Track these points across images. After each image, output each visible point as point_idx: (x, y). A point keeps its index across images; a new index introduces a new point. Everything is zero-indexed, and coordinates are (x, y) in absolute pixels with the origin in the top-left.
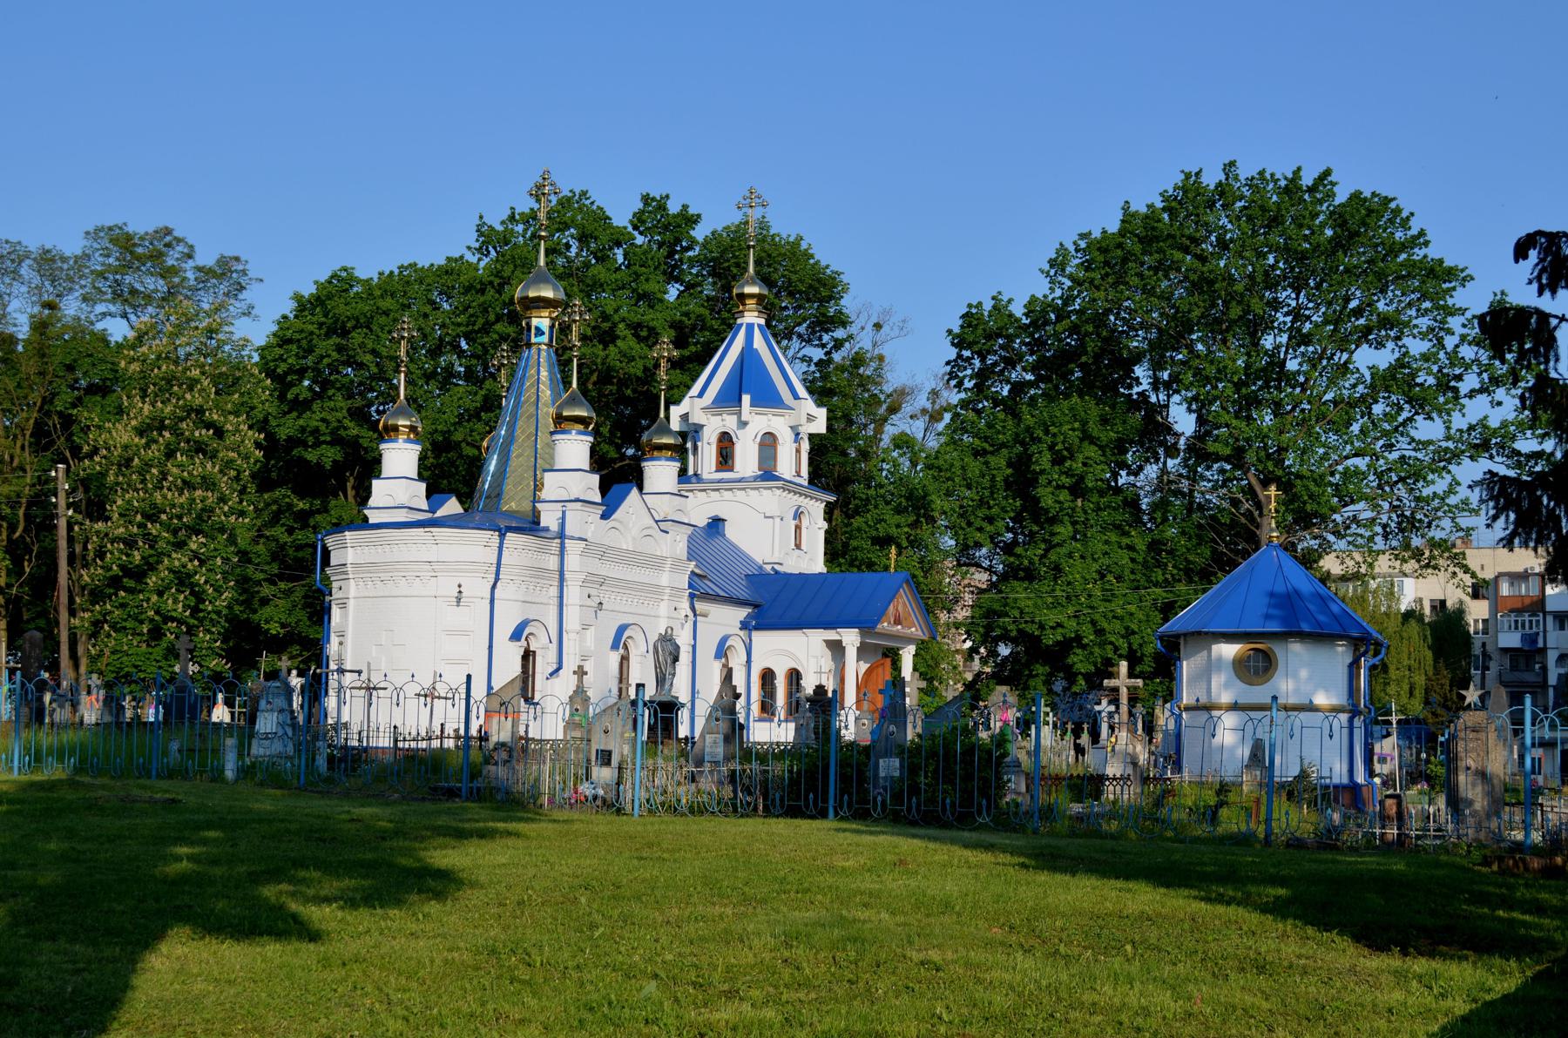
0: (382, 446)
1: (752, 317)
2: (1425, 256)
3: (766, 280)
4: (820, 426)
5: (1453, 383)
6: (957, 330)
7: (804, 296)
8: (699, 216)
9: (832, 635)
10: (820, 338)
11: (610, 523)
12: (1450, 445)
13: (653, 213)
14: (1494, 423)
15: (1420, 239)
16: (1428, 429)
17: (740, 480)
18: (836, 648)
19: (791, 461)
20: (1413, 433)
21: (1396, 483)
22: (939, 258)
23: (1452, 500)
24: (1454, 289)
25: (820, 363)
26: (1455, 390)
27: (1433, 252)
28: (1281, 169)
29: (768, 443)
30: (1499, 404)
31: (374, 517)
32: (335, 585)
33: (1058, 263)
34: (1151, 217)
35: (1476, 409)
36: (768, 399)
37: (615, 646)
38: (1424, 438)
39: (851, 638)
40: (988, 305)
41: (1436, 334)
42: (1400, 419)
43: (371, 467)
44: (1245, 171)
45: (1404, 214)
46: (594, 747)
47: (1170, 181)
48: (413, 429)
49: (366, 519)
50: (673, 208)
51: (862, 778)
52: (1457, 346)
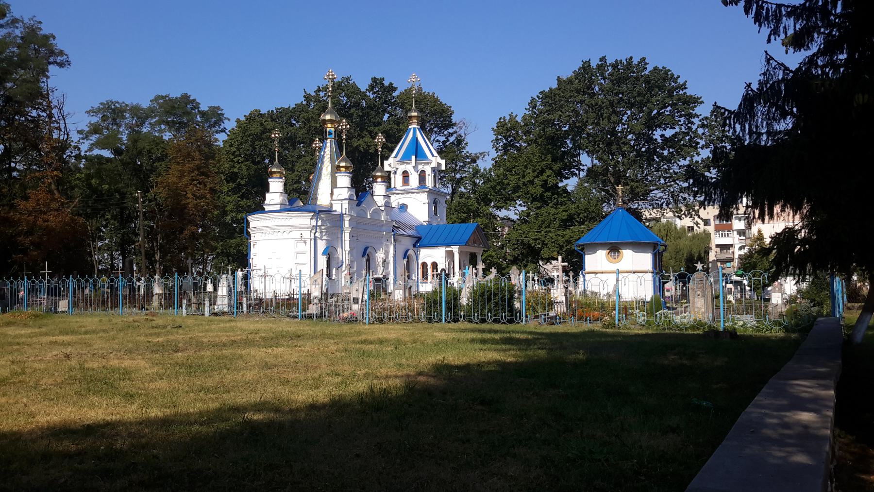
1: (414, 126)
3: (421, 111)
7: (437, 118)
9: (449, 249)
13: (376, 83)
15: (683, 87)
18: (450, 255)
22: (489, 101)
25: (444, 142)
27: (689, 92)
28: (623, 58)
29: (422, 176)
31: (267, 208)
33: (158, 98)
34: (570, 81)
37: (363, 256)
39: (455, 249)
40: (508, 118)
44: (610, 60)
47: (577, 65)
49: (264, 209)
50: (386, 83)
51: (455, 306)
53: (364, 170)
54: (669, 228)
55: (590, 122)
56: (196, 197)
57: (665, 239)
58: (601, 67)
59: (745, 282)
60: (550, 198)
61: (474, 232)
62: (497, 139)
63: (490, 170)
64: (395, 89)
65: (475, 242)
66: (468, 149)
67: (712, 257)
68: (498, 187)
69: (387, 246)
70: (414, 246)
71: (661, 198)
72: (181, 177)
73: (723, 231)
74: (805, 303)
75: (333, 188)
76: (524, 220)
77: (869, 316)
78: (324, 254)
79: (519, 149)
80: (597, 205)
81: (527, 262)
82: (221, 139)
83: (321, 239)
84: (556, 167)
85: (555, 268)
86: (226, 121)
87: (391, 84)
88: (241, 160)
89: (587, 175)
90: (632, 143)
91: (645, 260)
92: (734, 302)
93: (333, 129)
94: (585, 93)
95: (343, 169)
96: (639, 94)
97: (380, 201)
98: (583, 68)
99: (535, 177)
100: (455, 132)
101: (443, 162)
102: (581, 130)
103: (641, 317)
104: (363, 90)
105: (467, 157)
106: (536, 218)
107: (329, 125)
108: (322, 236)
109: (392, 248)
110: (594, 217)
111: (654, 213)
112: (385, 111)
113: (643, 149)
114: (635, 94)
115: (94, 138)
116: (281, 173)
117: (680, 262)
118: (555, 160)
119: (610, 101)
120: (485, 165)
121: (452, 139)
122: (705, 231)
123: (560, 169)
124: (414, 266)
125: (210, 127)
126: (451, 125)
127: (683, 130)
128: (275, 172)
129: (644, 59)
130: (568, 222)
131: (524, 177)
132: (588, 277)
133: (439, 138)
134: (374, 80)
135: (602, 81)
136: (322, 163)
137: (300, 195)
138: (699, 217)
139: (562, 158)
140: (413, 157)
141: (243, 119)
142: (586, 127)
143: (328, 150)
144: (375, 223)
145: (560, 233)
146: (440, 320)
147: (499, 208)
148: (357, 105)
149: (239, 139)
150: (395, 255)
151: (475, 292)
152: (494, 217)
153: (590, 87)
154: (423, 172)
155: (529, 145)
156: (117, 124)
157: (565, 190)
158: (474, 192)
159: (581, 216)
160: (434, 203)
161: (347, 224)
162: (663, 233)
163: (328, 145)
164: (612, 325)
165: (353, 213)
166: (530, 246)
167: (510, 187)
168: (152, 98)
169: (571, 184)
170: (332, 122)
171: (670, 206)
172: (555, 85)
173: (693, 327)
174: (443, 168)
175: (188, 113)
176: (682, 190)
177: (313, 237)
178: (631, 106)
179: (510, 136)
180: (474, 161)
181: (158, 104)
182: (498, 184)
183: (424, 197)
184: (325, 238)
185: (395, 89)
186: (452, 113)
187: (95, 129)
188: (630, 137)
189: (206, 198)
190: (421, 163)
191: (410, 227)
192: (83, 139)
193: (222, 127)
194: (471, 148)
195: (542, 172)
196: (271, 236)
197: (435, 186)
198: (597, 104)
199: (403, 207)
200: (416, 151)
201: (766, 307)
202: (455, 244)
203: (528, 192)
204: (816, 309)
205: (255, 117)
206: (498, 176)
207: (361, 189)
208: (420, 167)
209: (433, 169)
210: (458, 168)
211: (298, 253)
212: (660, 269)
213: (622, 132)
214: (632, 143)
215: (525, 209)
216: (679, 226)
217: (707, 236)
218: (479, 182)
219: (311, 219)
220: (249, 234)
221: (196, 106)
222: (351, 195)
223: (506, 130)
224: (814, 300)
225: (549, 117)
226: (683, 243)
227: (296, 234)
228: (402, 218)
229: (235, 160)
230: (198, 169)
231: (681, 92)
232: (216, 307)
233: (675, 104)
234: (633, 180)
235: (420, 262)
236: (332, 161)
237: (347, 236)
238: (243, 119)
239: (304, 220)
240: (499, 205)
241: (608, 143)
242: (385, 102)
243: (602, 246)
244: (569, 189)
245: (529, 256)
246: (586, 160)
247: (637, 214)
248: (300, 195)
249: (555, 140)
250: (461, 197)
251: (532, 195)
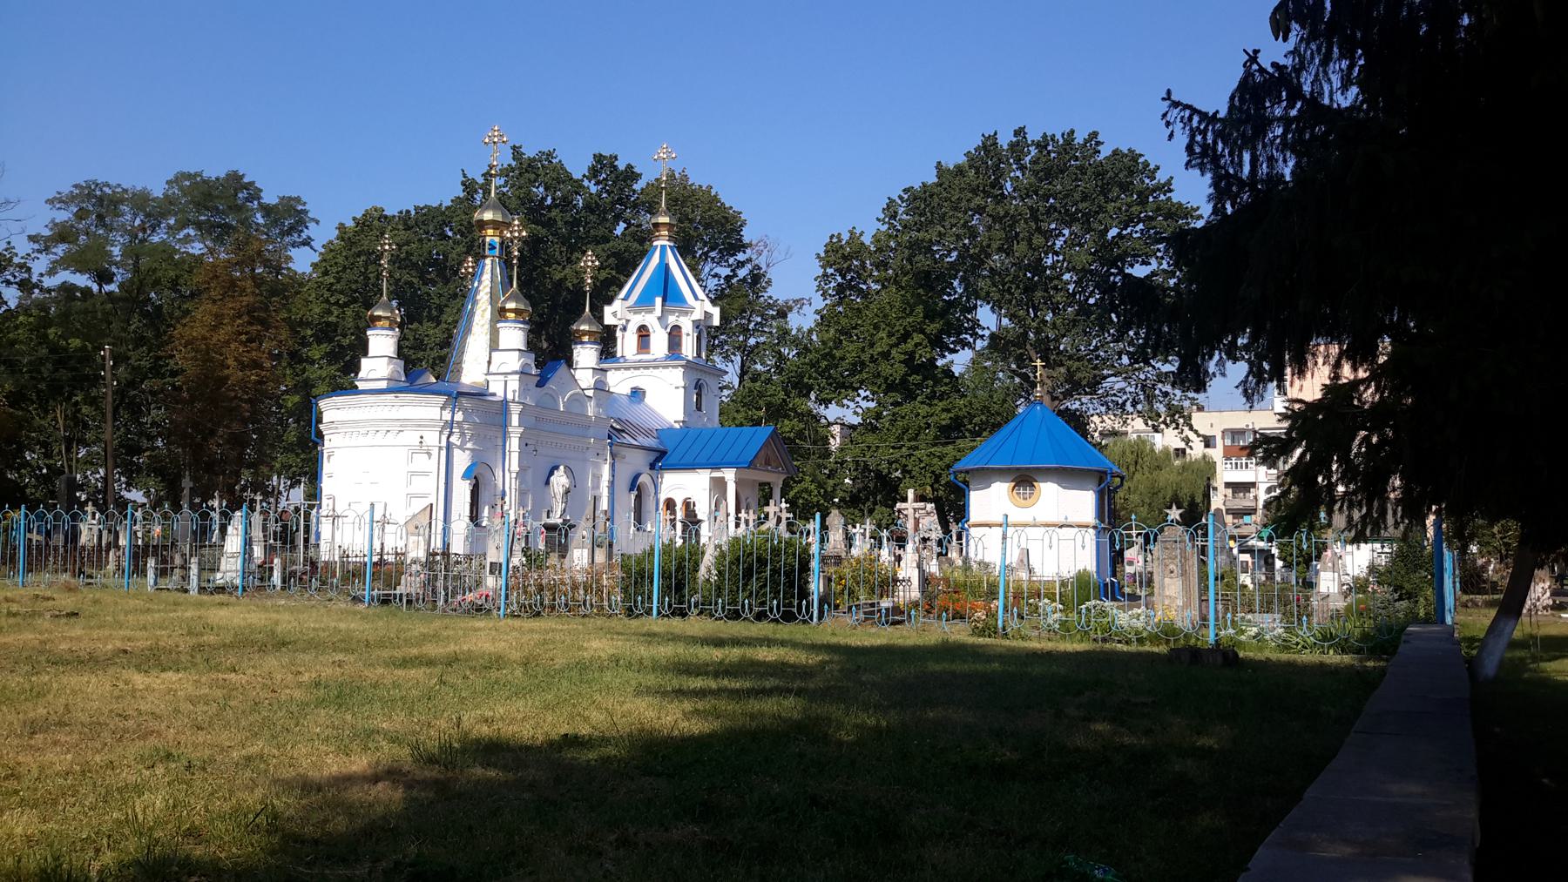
1: (662, 241)
7: (709, 231)
9: (717, 474)
11: (545, 389)
13: (602, 165)
18: (719, 486)
22: (810, 208)
25: (728, 278)
27: (1176, 197)
28: (1057, 130)
29: (675, 335)
31: (361, 386)
34: (960, 171)
37: (631, 489)
39: (729, 475)
40: (846, 237)
43: (362, 348)
44: (1034, 135)
45: (1152, 167)
46: (489, 560)
53: (557, 322)
54: (1140, 451)
55: (995, 246)
56: (243, 367)
57: (1132, 469)
58: (1017, 148)
59: (1275, 551)
60: (919, 386)
61: (766, 444)
62: (825, 275)
63: (810, 331)
64: (636, 177)
65: (767, 463)
66: (771, 291)
67: (1217, 502)
68: (824, 364)
69: (597, 466)
70: (652, 466)
71: (1122, 391)
72: (215, 328)
73: (1239, 458)
74: (1383, 592)
75: (492, 352)
76: (870, 425)
77: (1511, 623)
78: (465, 476)
79: (865, 295)
80: (1005, 401)
81: (875, 503)
82: (302, 261)
83: (462, 448)
84: (933, 328)
85: (916, 513)
86: (311, 225)
87: (630, 167)
88: (343, 299)
89: (990, 347)
90: (1071, 287)
91: (1082, 503)
92: (1251, 586)
93: (497, 239)
94: (987, 194)
95: (512, 315)
96: (1085, 198)
97: (585, 378)
98: (984, 147)
99: (892, 346)
100: (749, 260)
101: (716, 312)
102: (979, 260)
103: (1052, 613)
104: (577, 175)
105: (770, 306)
106: (893, 422)
107: (490, 232)
108: (464, 443)
109: (606, 471)
110: (994, 420)
111: (1110, 422)
112: (618, 218)
113: (1091, 301)
114: (1077, 196)
115: (60, 250)
117: (1137, 503)
118: (930, 315)
119: (1031, 208)
120: (802, 321)
121: (742, 273)
122: (1204, 456)
123: (941, 332)
124: (649, 504)
125: (283, 234)
126: (741, 246)
127: (1165, 266)
128: (379, 318)
129: (1094, 135)
130: (951, 431)
131: (872, 345)
132: (973, 531)
133: (718, 270)
134: (599, 158)
135: (1018, 173)
136: (475, 303)
137: (428, 361)
138: (1191, 428)
139: (943, 314)
140: (659, 300)
141: (350, 224)
142: (989, 256)
143: (486, 277)
144: (575, 423)
145: (937, 450)
146: (649, 612)
147: (826, 402)
148: (565, 204)
149: (340, 260)
150: (612, 484)
151: (722, 555)
152: (816, 418)
153: (996, 184)
154: (677, 328)
155: (884, 287)
156: (104, 225)
157: (947, 372)
158: (779, 370)
159: (976, 420)
160: (697, 390)
161: (515, 420)
162: (1130, 458)
163: (488, 268)
164: (988, 629)
165: (528, 401)
166: (879, 474)
167: (845, 364)
168: (171, 177)
169: (960, 361)
170: (495, 224)
171: (1139, 407)
172: (932, 178)
173: (1154, 639)
174: (716, 322)
175: (238, 209)
176: (1162, 378)
177: (444, 444)
178: (1069, 220)
179: (849, 269)
180: (782, 314)
181: (181, 189)
182: (824, 357)
183: (676, 376)
184: (469, 445)
186: (744, 223)
187: (63, 234)
188: (1067, 277)
189: (262, 368)
190: (673, 312)
191: (647, 433)
192: (39, 251)
193: (304, 235)
194: (778, 292)
195: (906, 337)
196: (362, 441)
197: (699, 355)
198: (1007, 214)
199: (637, 394)
200: (666, 288)
201: (1307, 598)
202: (729, 465)
203: (879, 375)
204: (1404, 604)
205: (373, 223)
206: (824, 343)
207: (549, 350)
208: (672, 320)
209: (697, 325)
210: (751, 326)
211: (413, 474)
212: (1111, 516)
213: (1053, 267)
214: (1071, 287)
215: (872, 405)
216: (1159, 447)
217: (1208, 468)
218: (790, 352)
219: (442, 408)
220: (320, 435)
221: (255, 194)
222: (525, 365)
223: (843, 259)
224: (1402, 588)
225: (921, 235)
226: (1166, 478)
227: (411, 437)
228: (634, 414)
229: (332, 300)
230: (249, 313)
231: (1162, 197)
232: (219, 575)
233: (1152, 219)
234: (1070, 358)
235: (663, 497)
236: (493, 298)
237: (514, 444)
238: (350, 224)
239: (428, 409)
240: (824, 396)
241: (1026, 288)
242: (620, 201)
244: (957, 370)
245: (875, 495)
246: (987, 317)
247: (1078, 422)
248: (428, 361)
249: (930, 281)
250: (754, 380)
251: (886, 379)
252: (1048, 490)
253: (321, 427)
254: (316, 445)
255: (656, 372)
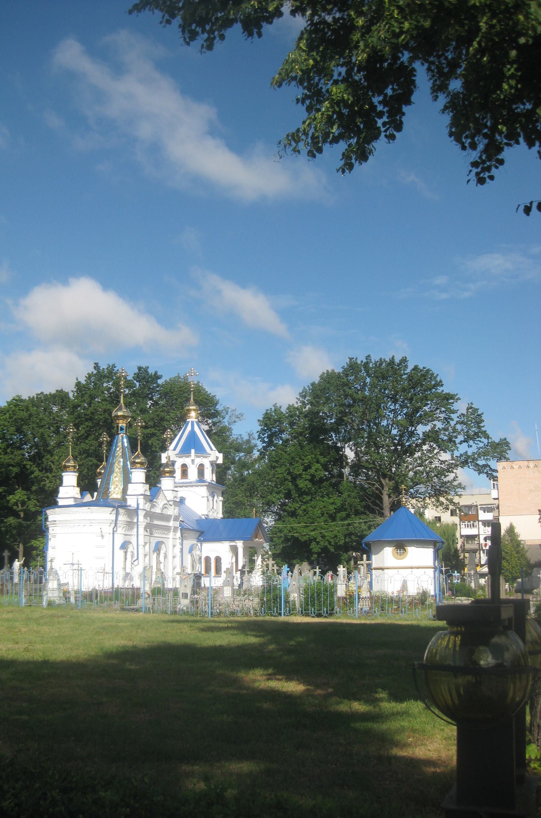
0: (63, 474)
2: (443, 391)
4: (220, 461)
5: (454, 439)
6: (261, 419)
7: (208, 407)
8: (162, 376)
10: (207, 421)
12: (453, 462)
14: (469, 453)
16: (445, 456)
17: (190, 483)
18: (234, 550)
19: (209, 476)
20: (440, 458)
21: (434, 476)
22: (259, 393)
23: (455, 483)
24: (453, 403)
26: (454, 442)
29: (201, 469)
30: (471, 446)
31: (61, 502)
32: (50, 528)
35: (463, 448)
36: (200, 451)
38: (443, 460)
39: (240, 544)
41: (447, 420)
42: (435, 452)
44: (375, 358)
48: (74, 467)
52: (455, 425)
101: (221, 456)
116: (74, 467)
128: (69, 467)
134: (140, 368)
170: (124, 417)
185: (160, 377)
209: (212, 463)
223: (271, 422)
239: (105, 514)
243: (389, 543)
252: (412, 550)
253: (48, 523)
254: (45, 532)
255: (191, 489)
